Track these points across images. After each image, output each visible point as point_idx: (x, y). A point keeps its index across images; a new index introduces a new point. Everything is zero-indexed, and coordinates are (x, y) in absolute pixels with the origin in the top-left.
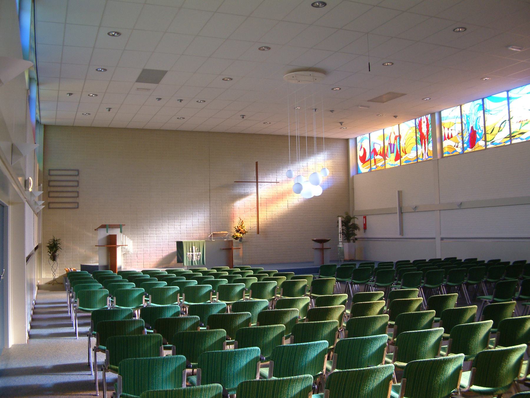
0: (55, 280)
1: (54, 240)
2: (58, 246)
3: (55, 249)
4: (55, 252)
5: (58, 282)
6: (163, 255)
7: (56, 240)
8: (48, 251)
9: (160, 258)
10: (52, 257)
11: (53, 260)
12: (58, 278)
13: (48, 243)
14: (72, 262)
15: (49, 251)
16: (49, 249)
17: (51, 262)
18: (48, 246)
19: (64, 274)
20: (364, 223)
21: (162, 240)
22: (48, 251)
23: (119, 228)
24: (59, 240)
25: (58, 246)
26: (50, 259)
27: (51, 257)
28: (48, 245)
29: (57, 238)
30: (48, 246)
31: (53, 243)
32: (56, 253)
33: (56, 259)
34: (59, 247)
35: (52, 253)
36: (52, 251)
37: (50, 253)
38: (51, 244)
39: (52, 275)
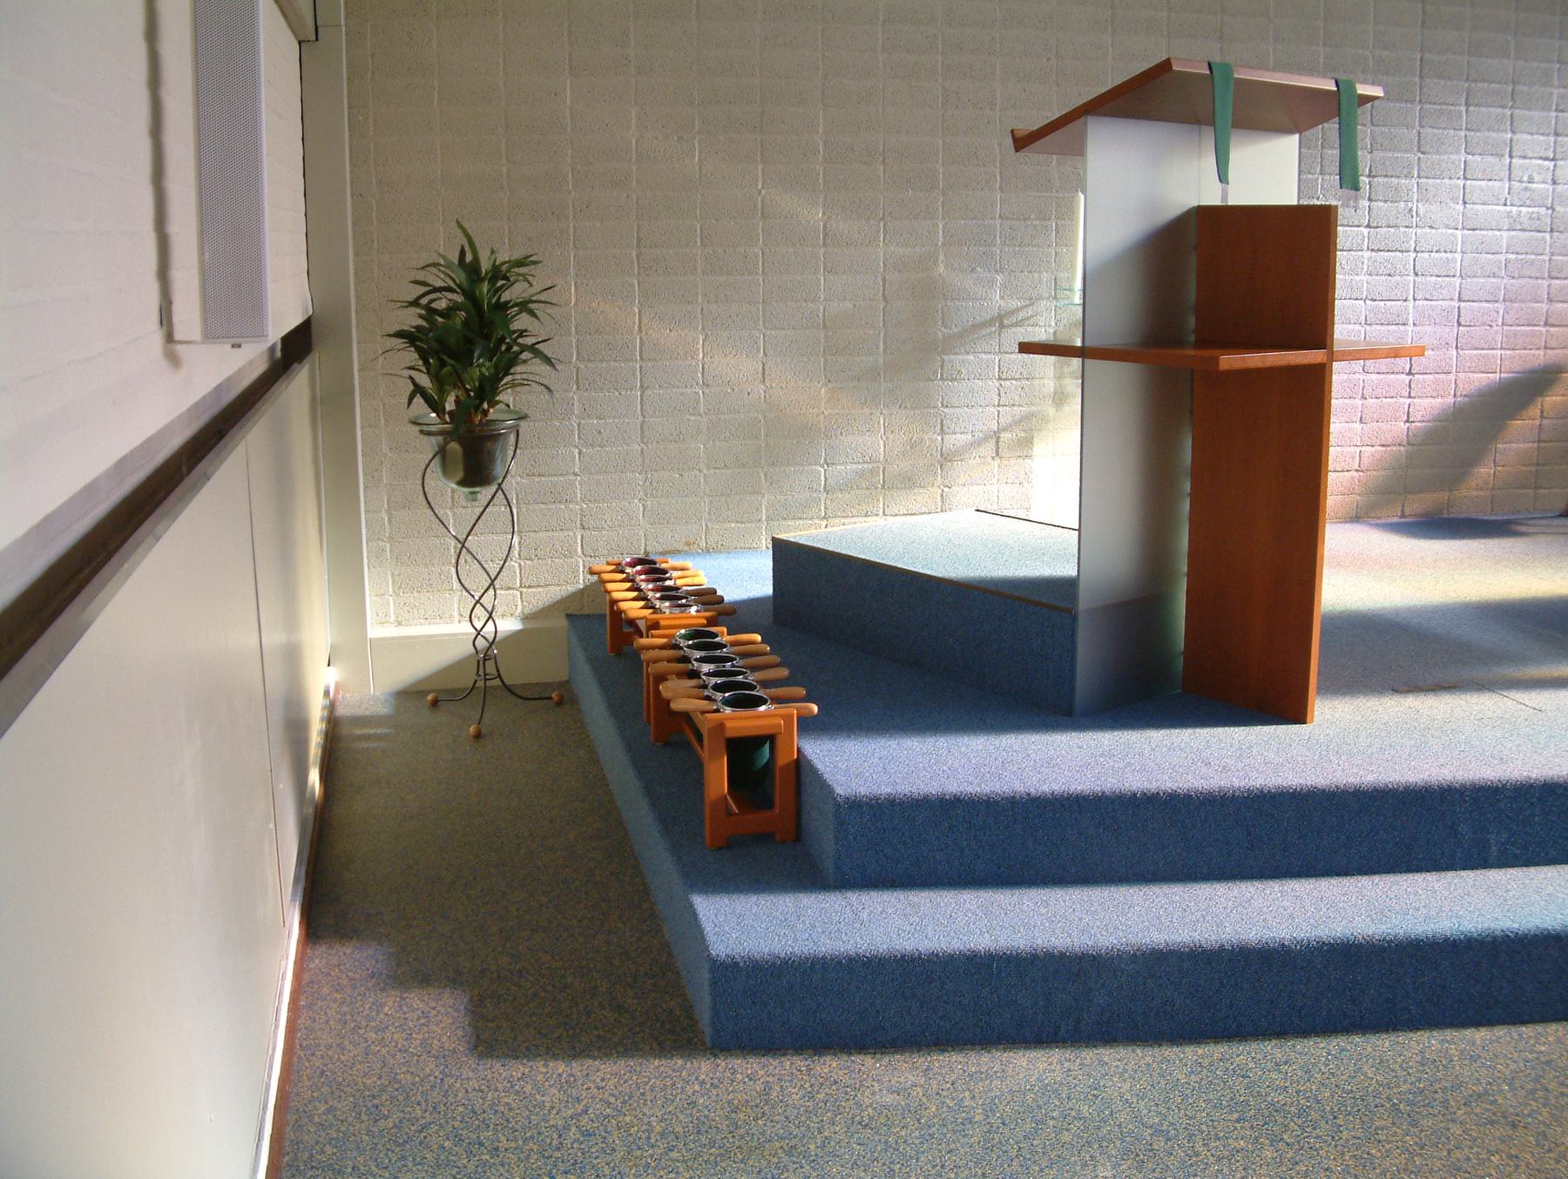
0: (486, 658)
1: (472, 270)
2: (515, 326)
3: (481, 366)
4: (487, 391)
5: (517, 284)
6: (1416, 415)
7: (485, 266)
8: (418, 390)
9: (1389, 439)
10: (454, 446)
11: (462, 483)
12: (514, 637)
13: (415, 303)
14: (640, 478)
15: (424, 381)
16: (424, 356)
17: (445, 489)
18: (410, 337)
19: (571, 589)
20: (406, 304)
21: (1411, 278)
22: (418, 390)
23: (1288, 131)
24: (520, 263)
25: (515, 326)
26: (436, 465)
27: (442, 452)
28: (411, 319)
29: (495, 248)
30: (410, 337)
31: (459, 298)
32: (493, 404)
33: (499, 470)
34: (529, 341)
35: (450, 405)
36: (458, 381)
37: (436, 406)
38: (447, 313)
39: (457, 602)
